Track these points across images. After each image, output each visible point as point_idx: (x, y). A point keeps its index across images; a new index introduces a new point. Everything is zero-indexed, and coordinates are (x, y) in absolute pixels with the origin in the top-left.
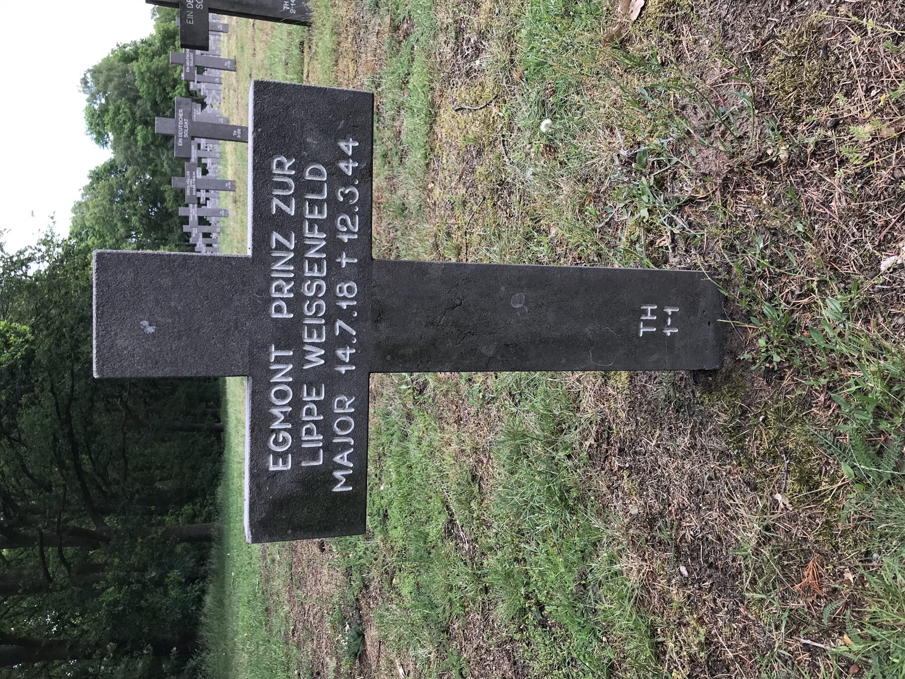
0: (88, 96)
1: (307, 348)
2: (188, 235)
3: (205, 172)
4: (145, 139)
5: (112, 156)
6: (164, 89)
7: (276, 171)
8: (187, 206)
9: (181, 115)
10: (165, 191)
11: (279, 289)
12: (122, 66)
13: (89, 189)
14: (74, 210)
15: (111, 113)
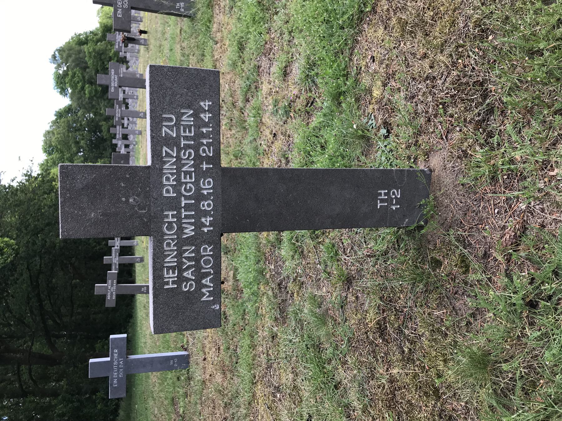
0: (55, 65)
1: (184, 225)
2: (116, 145)
3: (127, 107)
4: (90, 93)
5: (70, 103)
6: (103, 63)
8: (115, 127)
9: (113, 73)
10: (102, 125)
12: (77, 48)
13: (55, 122)
14: (45, 136)
15: (69, 76)
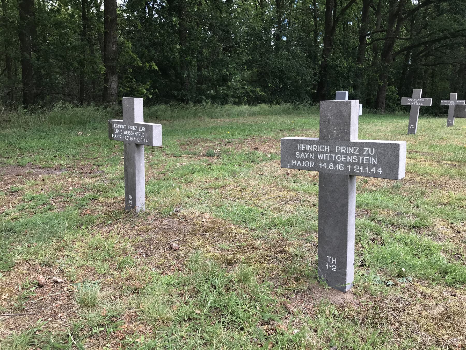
7: (342, 147)
11: (344, 149)
